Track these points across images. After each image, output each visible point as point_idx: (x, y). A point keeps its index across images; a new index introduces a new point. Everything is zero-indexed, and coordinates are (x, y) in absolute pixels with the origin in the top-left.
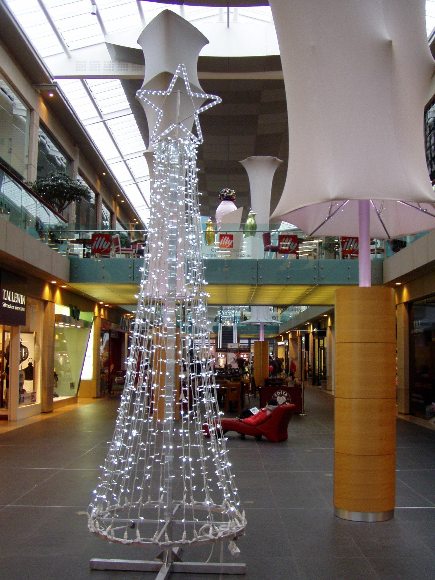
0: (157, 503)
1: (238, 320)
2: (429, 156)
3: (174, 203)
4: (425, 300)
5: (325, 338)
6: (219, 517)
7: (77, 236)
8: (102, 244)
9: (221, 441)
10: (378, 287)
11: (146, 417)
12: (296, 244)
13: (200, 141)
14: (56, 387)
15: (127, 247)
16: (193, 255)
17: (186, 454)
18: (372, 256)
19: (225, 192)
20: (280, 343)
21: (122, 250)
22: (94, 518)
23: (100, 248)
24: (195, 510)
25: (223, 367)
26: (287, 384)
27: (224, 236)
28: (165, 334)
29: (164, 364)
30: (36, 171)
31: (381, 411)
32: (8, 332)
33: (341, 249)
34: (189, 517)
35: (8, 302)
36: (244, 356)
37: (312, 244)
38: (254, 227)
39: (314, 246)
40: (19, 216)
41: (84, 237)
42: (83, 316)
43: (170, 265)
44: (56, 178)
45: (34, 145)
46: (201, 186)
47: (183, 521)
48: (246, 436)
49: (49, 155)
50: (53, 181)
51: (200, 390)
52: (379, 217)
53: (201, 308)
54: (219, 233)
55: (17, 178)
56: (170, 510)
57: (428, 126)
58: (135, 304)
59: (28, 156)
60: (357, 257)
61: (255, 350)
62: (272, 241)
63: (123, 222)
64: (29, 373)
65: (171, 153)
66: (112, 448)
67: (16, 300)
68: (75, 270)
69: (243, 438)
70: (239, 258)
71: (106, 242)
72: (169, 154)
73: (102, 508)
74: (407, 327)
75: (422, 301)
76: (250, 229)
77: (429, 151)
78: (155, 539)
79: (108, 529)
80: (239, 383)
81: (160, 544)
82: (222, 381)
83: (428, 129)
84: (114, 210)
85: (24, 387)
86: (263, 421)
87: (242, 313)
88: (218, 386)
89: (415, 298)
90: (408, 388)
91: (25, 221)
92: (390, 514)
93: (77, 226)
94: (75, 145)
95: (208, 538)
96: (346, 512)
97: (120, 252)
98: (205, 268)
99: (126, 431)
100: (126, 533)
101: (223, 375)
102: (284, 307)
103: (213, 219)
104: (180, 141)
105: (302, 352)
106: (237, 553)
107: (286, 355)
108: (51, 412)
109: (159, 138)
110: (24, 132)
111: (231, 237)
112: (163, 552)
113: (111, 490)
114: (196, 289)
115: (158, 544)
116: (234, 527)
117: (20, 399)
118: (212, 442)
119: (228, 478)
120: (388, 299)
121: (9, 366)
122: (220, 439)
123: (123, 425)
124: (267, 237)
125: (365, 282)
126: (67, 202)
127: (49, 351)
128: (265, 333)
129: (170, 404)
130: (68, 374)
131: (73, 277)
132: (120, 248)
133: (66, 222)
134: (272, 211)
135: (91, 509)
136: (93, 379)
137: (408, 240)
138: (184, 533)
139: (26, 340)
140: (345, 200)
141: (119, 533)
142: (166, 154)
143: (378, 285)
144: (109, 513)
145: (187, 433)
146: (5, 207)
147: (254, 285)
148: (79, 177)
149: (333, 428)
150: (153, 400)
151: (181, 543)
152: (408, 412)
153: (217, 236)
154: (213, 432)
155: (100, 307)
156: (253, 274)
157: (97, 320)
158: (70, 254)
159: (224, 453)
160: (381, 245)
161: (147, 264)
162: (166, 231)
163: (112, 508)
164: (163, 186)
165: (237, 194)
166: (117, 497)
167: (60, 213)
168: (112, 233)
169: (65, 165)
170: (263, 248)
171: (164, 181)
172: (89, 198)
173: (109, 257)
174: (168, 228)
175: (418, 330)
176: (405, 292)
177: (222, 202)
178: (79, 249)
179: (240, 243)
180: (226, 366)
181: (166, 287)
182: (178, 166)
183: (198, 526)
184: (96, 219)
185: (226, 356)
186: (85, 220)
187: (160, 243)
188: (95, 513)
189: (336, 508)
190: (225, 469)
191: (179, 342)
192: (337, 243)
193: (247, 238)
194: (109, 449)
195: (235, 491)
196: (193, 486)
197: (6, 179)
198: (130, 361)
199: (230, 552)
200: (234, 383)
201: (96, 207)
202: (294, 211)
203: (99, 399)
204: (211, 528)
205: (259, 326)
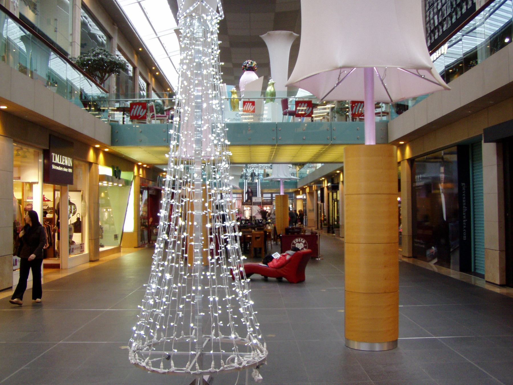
0: (189, 337)
1: (261, 177)
2: (429, 29)
3: (199, 72)
4: (425, 157)
5: (338, 192)
6: (243, 349)
7: (117, 105)
8: (138, 111)
9: (244, 282)
10: (384, 145)
11: (177, 262)
12: (311, 108)
13: (221, 16)
14: (102, 238)
15: (162, 114)
16: (217, 118)
17: (214, 294)
18: (378, 119)
19: (248, 63)
20: (298, 197)
21: (157, 117)
22: (134, 351)
23: (138, 115)
24: (222, 343)
25: (248, 218)
26: (305, 232)
27: (247, 102)
28: (193, 189)
29: (192, 215)
30: (79, 47)
31: (385, 254)
32: (58, 190)
33: (350, 112)
34: (216, 349)
35: (57, 165)
36: (267, 208)
37: (325, 109)
38: (273, 94)
39: (328, 110)
40: (64, 87)
41: (123, 105)
42: (124, 175)
43: (196, 128)
44: (97, 53)
45: (77, 24)
46: (223, 57)
47: (212, 352)
48: (269, 278)
49: (91, 33)
50: (94, 56)
51: (225, 237)
52: (383, 83)
53: (224, 165)
54: (242, 100)
55: (63, 54)
56: (200, 343)
57: (427, 2)
58: (166, 164)
59: (72, 35)
60: (363, 119)
61: (276, 203)
62: (289, 106)
63: (158, 92)
64: (78, 227)
65: (195, 28)
66: (148, 289)
67: (64, 162)
68: (116, 135)
69: (266, 280)
70: (261, 122)
71: (142, 110)
72: (194, 29)
73: (141, 343)
74: (410, 180)
75: (422, 158)
76: (270, 96)
77: (428, 25)
78: (188, 368)
79: (146, 360)
80: (262, 232)
81: (192, 372)
82: (248, 230)
83: (428, 5)
84: (149, 81)
85: (74, 239)
86: (283, 265)
87: (265, 170)
88: (241, 234)
89: (416, 155)
90: (411, 234)
91: (71, 92)
92: (394, 343)
93: (118, 96)
94: (114, 24)
95: (234, 367)
96: (356, 343)
97: (156, 118)
98: (227, 129)
99: (160, 274)
100: (162, 364)
101: (245, 225)
102: (302, 165)
103: (238, 88)
104: (203, 18)
105: (318, 204)
106: (259, 380)
107: (305, 206)
108: (97, 260)
109: (185, 15)
110: (68, 12)
111: (253, 103)
112: (195, 380)
113: (149, 326)
114: (219, 149)
115: (190, 373)
116: (256, 357)
117: (70, 250)
118: (236, 283)
119: (250, 315)
120: (391, 155)
121: (59, 221)
122: (243, 281)
123: (157, 270)
124: (285, 103)
125: (370, 140)
126: (107, 75)
127: (95, 208)
128: (285, 188)
129: (198, 250)
130: (112, 227)
131: (115, 140)
132: (155, 115)
133: (107, 92)
134: (288, 79)
135: (131, 343)
136: (134, 231)
137: (410, 104)
138: (213, 363)
139: (74, 197)
140: (352, 67)
141: (156, 364)
142: (191, 29)
143: (384, 143)
144: (148, 347)
145: (214, 275)
146: (53, 80)
147: (275, 145)
148: (118, 53)
149: (343, 270)
150: (183, 247)
151: (210, 372)
152: (411, 255)
153: (241, 103)
154: (236, 274)
155: (139, 167)
156: (273, 136)
157: (137, 178)
158: (111, 121)
159: (247, 293)
160: (386, 108)
161: (176, 127)
162: (192, 97)
163: (150, 343)
164: (188, 57)
165: (258, 65)
166: (153, 333)
167: (101, 84)
168: (148, 101)
169: (105, 42)
170: (282, 112)
171: (190, 53)
172: (126, 71)
173: (145, 123)
174: (193, 95)
175: (420, 183)
176: (408, 150)
177: (246, 72)
178: (118, 116)
179: (261, 108)
180: (251, 217)
181: (193, 147)
182: (202, 40)
183: (225, 357)
184: (134, 89)
185: (251, 209)
186: (124, 89)
187: (186, 108)
188: (135, 347)
189: (347, 340)
190: (248, 307)
191: (205, 194)
192: (348, 108)
193: (267, 104)
194: (145, 291)
195: (257, 326)
196: (219, 322)
197: (53, 55)
198: (163, 213)
199: (254, 378)
200: (257, 232)
201: (133, 79)
202: (308, 77)
203: (140, 249)
204: (236, 358)
205: (279, 181)
